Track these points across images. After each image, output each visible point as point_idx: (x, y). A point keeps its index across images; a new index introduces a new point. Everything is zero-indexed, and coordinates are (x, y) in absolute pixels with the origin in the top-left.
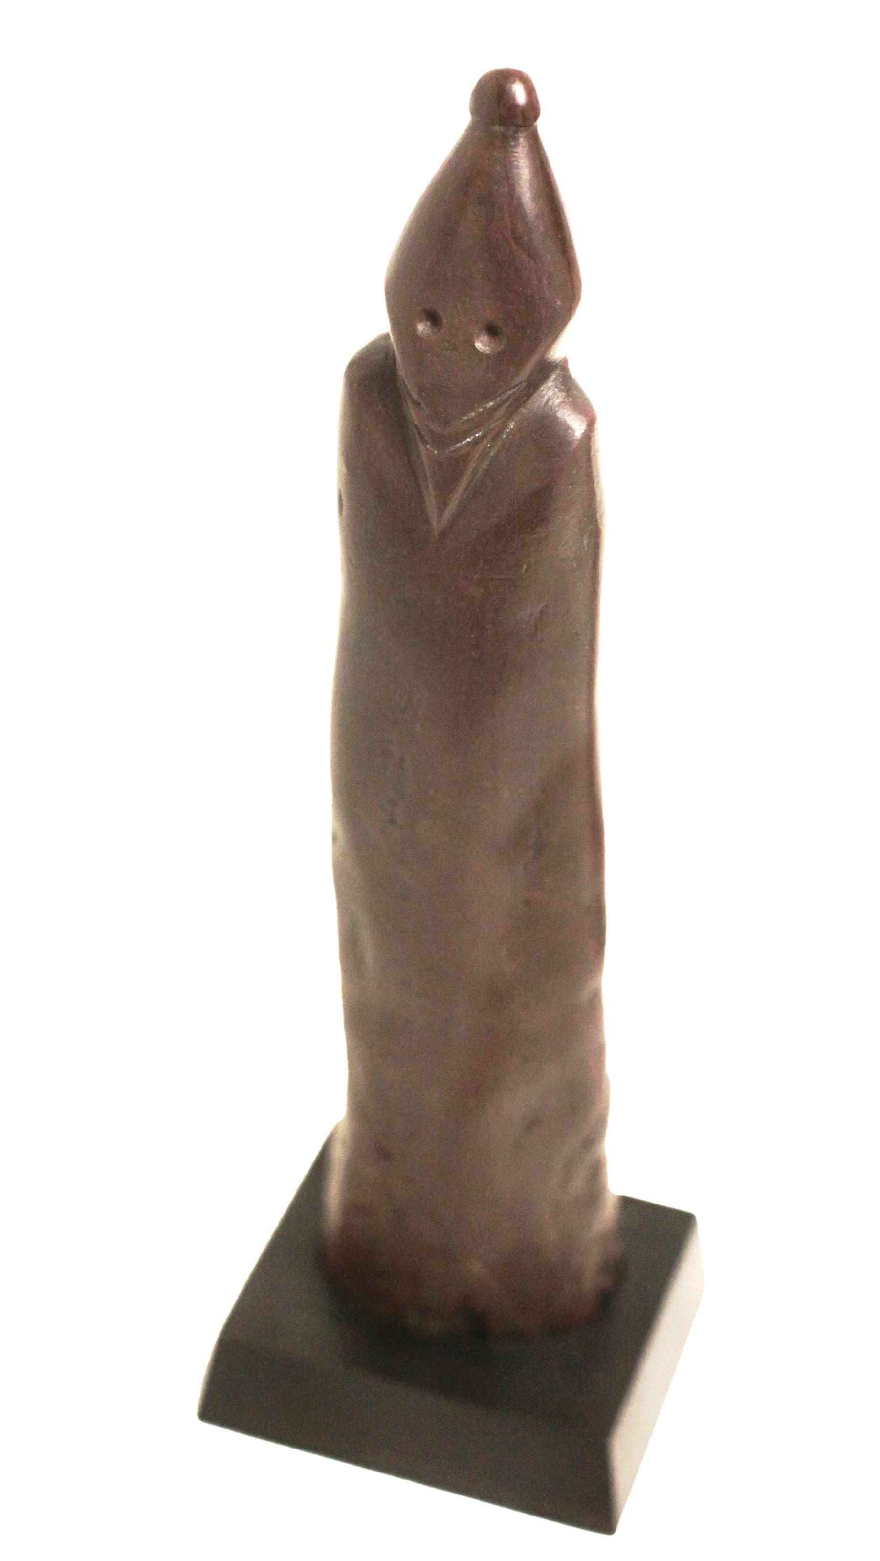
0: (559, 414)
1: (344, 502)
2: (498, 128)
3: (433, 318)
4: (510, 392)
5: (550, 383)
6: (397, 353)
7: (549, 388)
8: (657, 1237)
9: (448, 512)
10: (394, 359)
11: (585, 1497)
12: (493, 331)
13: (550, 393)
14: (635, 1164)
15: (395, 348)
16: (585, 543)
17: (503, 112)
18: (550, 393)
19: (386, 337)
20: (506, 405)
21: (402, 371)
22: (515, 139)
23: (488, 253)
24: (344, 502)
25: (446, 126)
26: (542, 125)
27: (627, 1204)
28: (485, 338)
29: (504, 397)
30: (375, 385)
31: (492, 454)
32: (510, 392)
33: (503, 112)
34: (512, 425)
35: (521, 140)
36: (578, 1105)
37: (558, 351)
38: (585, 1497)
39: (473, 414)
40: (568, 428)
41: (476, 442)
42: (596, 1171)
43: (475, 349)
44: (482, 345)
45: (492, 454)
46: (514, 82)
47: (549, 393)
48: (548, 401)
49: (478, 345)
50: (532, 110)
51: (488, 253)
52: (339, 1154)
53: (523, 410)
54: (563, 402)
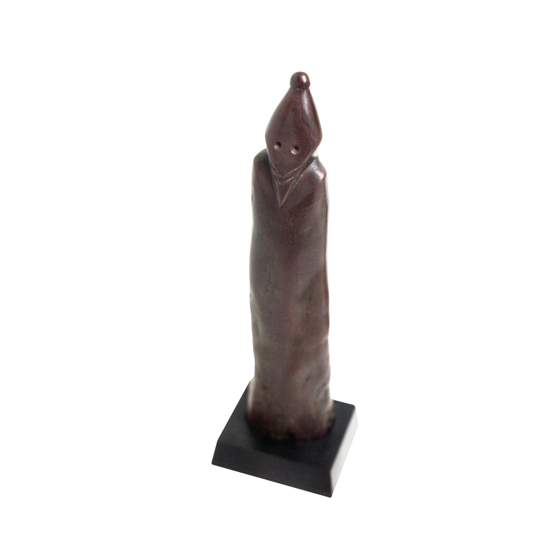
2: (298, 89)
3: (279, 144)
5: (313, 163)
8: (345, 412)
9: (284, 200)
12: (296, 148)
14: (338, 391)
17: (300, 84)
19: (266, 150)
21: (270, 160)
22: (303, 92)
23: (295, 126)
24: (260, 329)
26: (311, 88)
27: (335, 402)
30: (262, 165)
33: (300, 84)
34: (302, 175)
36: (321, 373)
37: (315, 154)
40: (318, 176)
41: (292, 180)
44: (293, 152)
47: (313, 166)
50: (308, 84)
51: (295, 126)
52: (252, 388)
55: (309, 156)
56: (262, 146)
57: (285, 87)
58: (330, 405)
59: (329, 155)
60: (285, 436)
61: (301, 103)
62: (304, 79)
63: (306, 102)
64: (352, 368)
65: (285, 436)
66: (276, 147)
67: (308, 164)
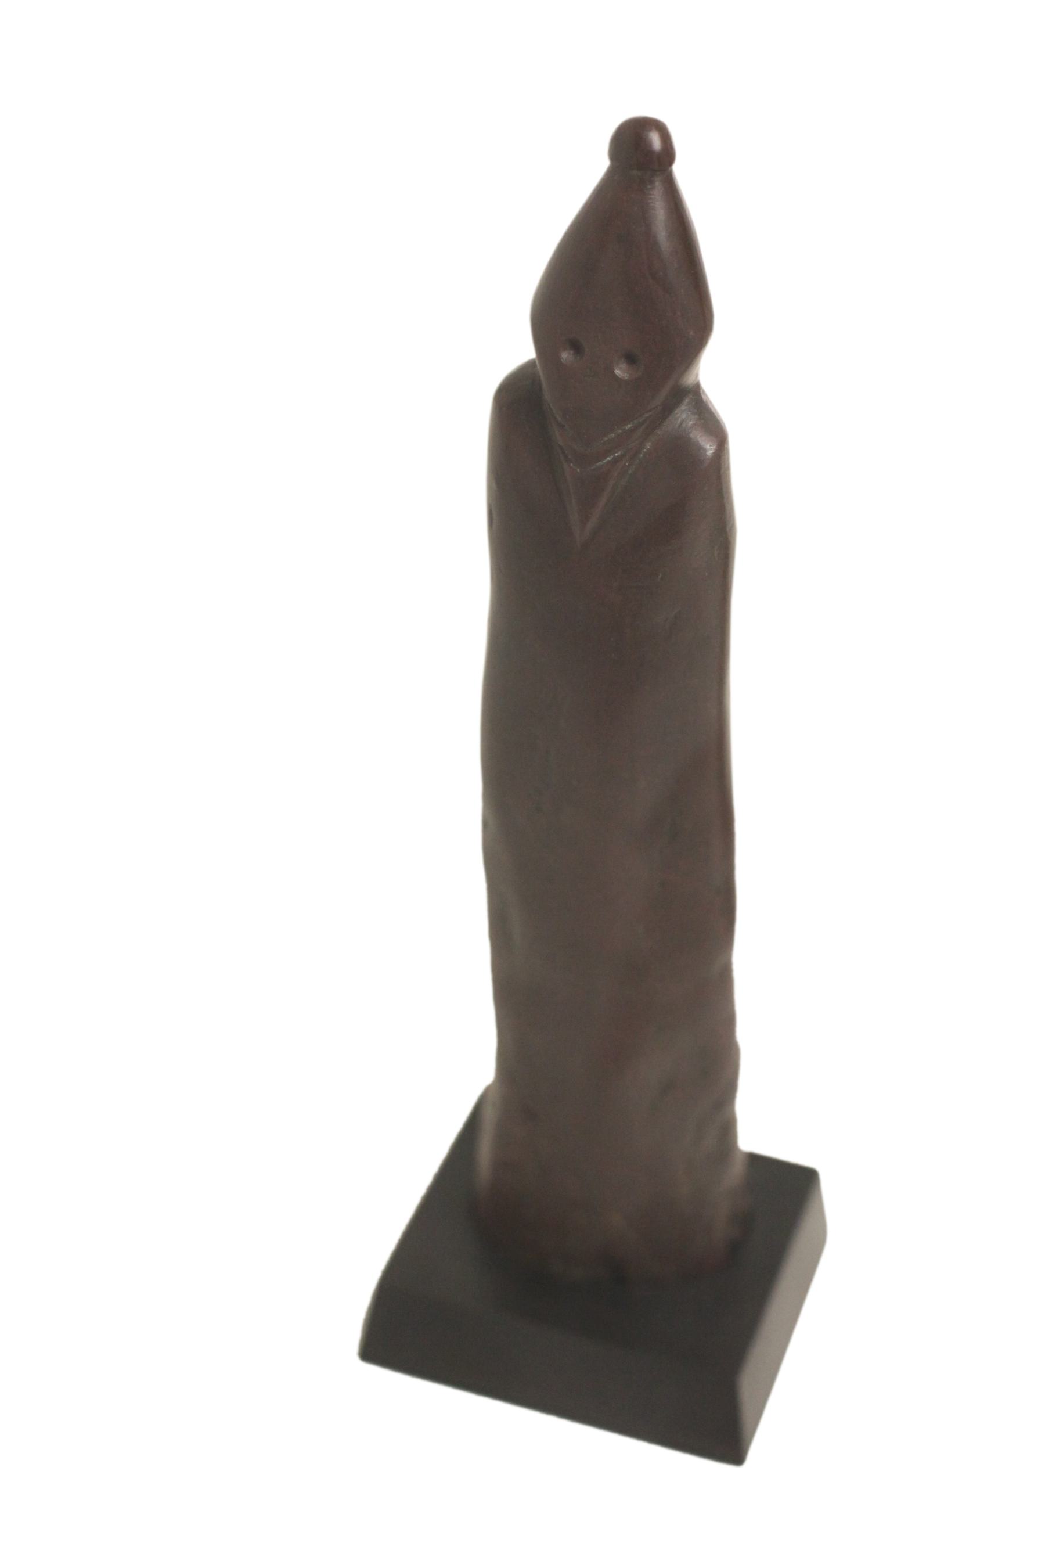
0: (692, 436)
1: (494, 516)
2: (635, 172)
3: (576, 347)
4: (647, 415)
5: (683, 407)
6: (542, 379)
7: (683, 412)
8: (787, 1192)
9: (591, 525)
10: (541, 389)
11: (722, 1436)
12: (631, 359)
13: (684, 416)
14: (764, 1123)
15: (541, 374)
16: (716, 553)
17: (641, 155)
18: (684, 416)
19: (531, 364)
20: (644, 427)
21: (547, 396)
22: (652, 182)
23: (627, 282)
24: (494, 516)
25: (585, 168)
26: (679, 170)
27: (755, 1160)
28: (624, 366)
29: (641, 420)
30: (520, 406)
31: (630, 472)
32: (647, 415)
33: (641, 155)
34: (648, 445)
35: (657, 184)
36: (713, 1066)
37: (689, 380)
38: (722, 1436)
39: (613, 435)
40: (700, 448)
41: (616, 461)
42: (728, 1129)
43: (615, 376)
44: (621, 371)
45: (630, 472)
46: (650, 130)
47: (683, 416)
48: (680, 425)
49: (618, 372)
50: (668, 154)
51: (627, 282)
52: (490, 1116)
53: (659, 432)
54: (695, 424)
55: (670, 383)
56: (520, 349)
57: (594, 166)
58: (737, 1170)
59: (737, 375)
60: (602, 1256)
61: (645, 216)
62: (655, 140)
63: (660, 212)
64: (814, 1047)
65: (602, 1256)
66: (566, 356)
67: (668, 409)
